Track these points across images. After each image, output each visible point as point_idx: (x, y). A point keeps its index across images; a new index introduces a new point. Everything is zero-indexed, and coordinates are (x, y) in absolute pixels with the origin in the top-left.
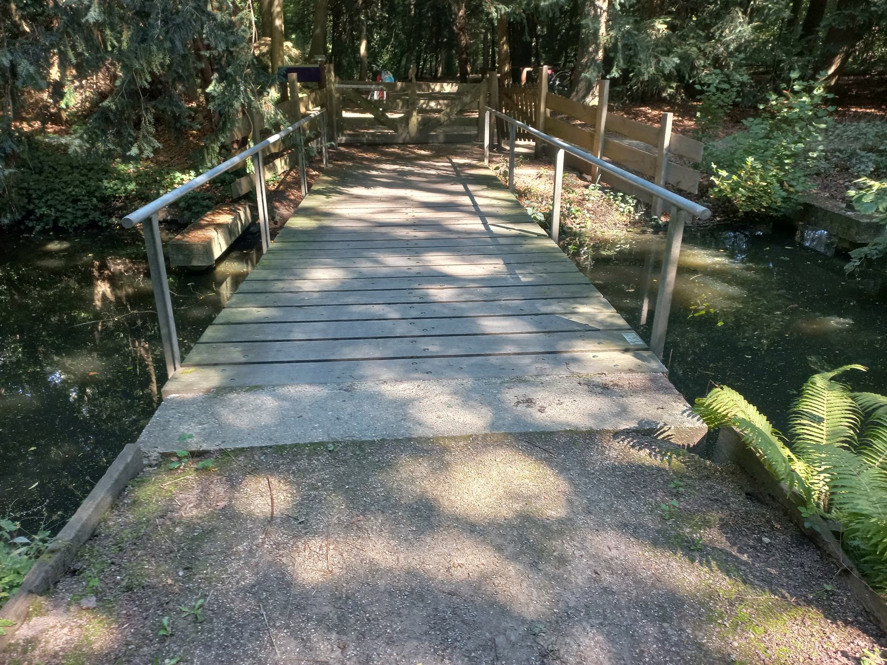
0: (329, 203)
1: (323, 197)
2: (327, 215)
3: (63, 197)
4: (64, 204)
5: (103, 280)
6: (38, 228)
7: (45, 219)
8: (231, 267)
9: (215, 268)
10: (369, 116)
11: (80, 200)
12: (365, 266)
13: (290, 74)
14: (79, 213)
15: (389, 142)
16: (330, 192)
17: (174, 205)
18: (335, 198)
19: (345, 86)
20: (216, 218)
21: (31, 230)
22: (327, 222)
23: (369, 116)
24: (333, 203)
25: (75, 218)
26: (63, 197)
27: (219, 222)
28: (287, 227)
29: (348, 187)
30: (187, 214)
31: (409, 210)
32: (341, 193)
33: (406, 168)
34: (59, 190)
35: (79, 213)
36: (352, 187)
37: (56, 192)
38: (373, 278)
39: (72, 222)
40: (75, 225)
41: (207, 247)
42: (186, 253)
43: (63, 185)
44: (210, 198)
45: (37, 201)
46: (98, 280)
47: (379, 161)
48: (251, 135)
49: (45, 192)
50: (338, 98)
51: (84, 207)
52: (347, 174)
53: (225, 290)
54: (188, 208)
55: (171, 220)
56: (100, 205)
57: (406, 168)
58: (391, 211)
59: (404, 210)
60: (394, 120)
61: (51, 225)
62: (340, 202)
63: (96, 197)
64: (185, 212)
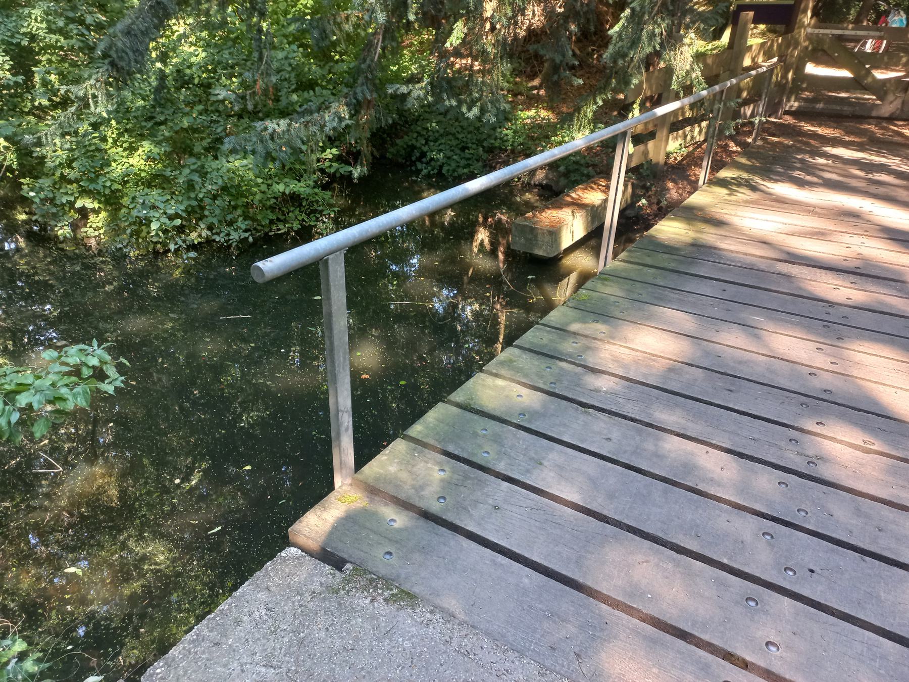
0: (728, 202)
1: (723, 191)
2: (718, 223)
3: (454, 143)
4: (452, 151)
5: (485, 227)
6: (425, 171)
7: (433, 163)
8: (582, 261)
9: (560, 259)
10: (845, 73)
11: (468, 148)
12: (732, 341)
13: (743, 14)
14: (463, 162)
15: (864, 117)
16: (739, 185)
17: (552, 166)
18: (744, 194)
19: (822, 31)
20: (586, 195)
21: (418, 172)
22: (710, 235)
23: (845, 73)
24: (737, 204)
25: (458, 166)
26: (454, 143)
27: (586, 201)
28: (652, 237)
29: (770, 179)
30: (563, 181)
31: (857, 240)
32: (754, 188)
33: (876, 159)
34: (454, 135)
35: (463, 162)
36: (776, 181)
37: (450, 137)
38: (731, 376)
39: (454, 171)
40: (456, 174)
41: (554, 233)
42: (530, 236)
43: (459, 129)
44: (594, 166)
45: (432, 144)
46: (480, 225)
47: (835, 142)
48: (638, 101)
49: (441, 135)
50: (807, 48)
51: (470, 156)
52: (776, 159)
53: (563, 291)
54: (566, 175)
55: (546, 185)
56: (485, 156)
57: (876, 159)
58: (819, 235)
59: (846, 238)
60: (885, 82)
61: (436, 171)
62: (748, 203)
63: (483, 147)
64: (562, 179)
